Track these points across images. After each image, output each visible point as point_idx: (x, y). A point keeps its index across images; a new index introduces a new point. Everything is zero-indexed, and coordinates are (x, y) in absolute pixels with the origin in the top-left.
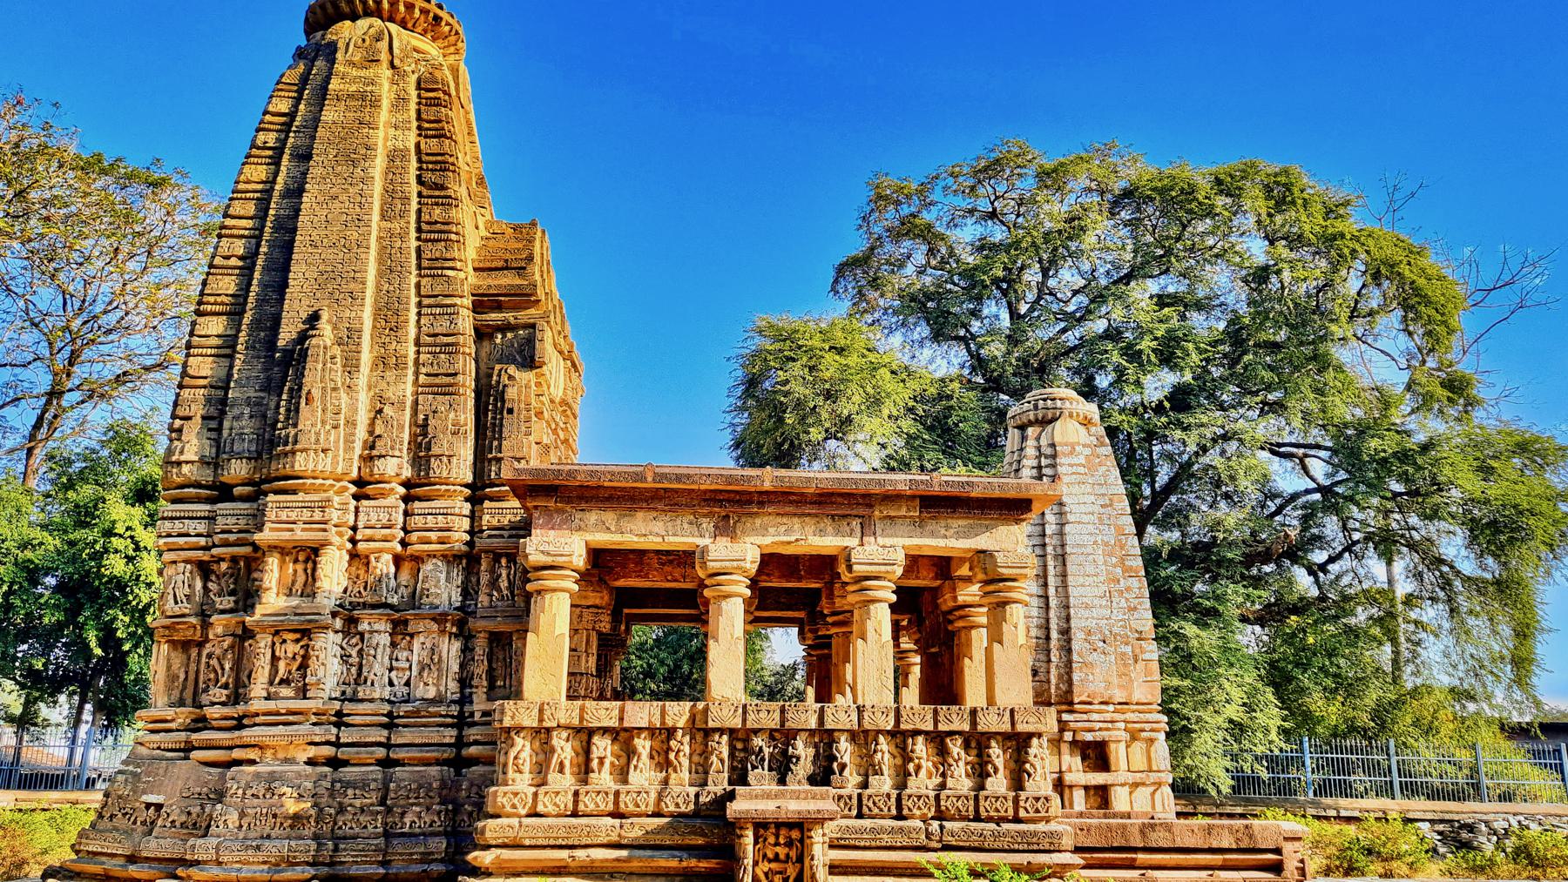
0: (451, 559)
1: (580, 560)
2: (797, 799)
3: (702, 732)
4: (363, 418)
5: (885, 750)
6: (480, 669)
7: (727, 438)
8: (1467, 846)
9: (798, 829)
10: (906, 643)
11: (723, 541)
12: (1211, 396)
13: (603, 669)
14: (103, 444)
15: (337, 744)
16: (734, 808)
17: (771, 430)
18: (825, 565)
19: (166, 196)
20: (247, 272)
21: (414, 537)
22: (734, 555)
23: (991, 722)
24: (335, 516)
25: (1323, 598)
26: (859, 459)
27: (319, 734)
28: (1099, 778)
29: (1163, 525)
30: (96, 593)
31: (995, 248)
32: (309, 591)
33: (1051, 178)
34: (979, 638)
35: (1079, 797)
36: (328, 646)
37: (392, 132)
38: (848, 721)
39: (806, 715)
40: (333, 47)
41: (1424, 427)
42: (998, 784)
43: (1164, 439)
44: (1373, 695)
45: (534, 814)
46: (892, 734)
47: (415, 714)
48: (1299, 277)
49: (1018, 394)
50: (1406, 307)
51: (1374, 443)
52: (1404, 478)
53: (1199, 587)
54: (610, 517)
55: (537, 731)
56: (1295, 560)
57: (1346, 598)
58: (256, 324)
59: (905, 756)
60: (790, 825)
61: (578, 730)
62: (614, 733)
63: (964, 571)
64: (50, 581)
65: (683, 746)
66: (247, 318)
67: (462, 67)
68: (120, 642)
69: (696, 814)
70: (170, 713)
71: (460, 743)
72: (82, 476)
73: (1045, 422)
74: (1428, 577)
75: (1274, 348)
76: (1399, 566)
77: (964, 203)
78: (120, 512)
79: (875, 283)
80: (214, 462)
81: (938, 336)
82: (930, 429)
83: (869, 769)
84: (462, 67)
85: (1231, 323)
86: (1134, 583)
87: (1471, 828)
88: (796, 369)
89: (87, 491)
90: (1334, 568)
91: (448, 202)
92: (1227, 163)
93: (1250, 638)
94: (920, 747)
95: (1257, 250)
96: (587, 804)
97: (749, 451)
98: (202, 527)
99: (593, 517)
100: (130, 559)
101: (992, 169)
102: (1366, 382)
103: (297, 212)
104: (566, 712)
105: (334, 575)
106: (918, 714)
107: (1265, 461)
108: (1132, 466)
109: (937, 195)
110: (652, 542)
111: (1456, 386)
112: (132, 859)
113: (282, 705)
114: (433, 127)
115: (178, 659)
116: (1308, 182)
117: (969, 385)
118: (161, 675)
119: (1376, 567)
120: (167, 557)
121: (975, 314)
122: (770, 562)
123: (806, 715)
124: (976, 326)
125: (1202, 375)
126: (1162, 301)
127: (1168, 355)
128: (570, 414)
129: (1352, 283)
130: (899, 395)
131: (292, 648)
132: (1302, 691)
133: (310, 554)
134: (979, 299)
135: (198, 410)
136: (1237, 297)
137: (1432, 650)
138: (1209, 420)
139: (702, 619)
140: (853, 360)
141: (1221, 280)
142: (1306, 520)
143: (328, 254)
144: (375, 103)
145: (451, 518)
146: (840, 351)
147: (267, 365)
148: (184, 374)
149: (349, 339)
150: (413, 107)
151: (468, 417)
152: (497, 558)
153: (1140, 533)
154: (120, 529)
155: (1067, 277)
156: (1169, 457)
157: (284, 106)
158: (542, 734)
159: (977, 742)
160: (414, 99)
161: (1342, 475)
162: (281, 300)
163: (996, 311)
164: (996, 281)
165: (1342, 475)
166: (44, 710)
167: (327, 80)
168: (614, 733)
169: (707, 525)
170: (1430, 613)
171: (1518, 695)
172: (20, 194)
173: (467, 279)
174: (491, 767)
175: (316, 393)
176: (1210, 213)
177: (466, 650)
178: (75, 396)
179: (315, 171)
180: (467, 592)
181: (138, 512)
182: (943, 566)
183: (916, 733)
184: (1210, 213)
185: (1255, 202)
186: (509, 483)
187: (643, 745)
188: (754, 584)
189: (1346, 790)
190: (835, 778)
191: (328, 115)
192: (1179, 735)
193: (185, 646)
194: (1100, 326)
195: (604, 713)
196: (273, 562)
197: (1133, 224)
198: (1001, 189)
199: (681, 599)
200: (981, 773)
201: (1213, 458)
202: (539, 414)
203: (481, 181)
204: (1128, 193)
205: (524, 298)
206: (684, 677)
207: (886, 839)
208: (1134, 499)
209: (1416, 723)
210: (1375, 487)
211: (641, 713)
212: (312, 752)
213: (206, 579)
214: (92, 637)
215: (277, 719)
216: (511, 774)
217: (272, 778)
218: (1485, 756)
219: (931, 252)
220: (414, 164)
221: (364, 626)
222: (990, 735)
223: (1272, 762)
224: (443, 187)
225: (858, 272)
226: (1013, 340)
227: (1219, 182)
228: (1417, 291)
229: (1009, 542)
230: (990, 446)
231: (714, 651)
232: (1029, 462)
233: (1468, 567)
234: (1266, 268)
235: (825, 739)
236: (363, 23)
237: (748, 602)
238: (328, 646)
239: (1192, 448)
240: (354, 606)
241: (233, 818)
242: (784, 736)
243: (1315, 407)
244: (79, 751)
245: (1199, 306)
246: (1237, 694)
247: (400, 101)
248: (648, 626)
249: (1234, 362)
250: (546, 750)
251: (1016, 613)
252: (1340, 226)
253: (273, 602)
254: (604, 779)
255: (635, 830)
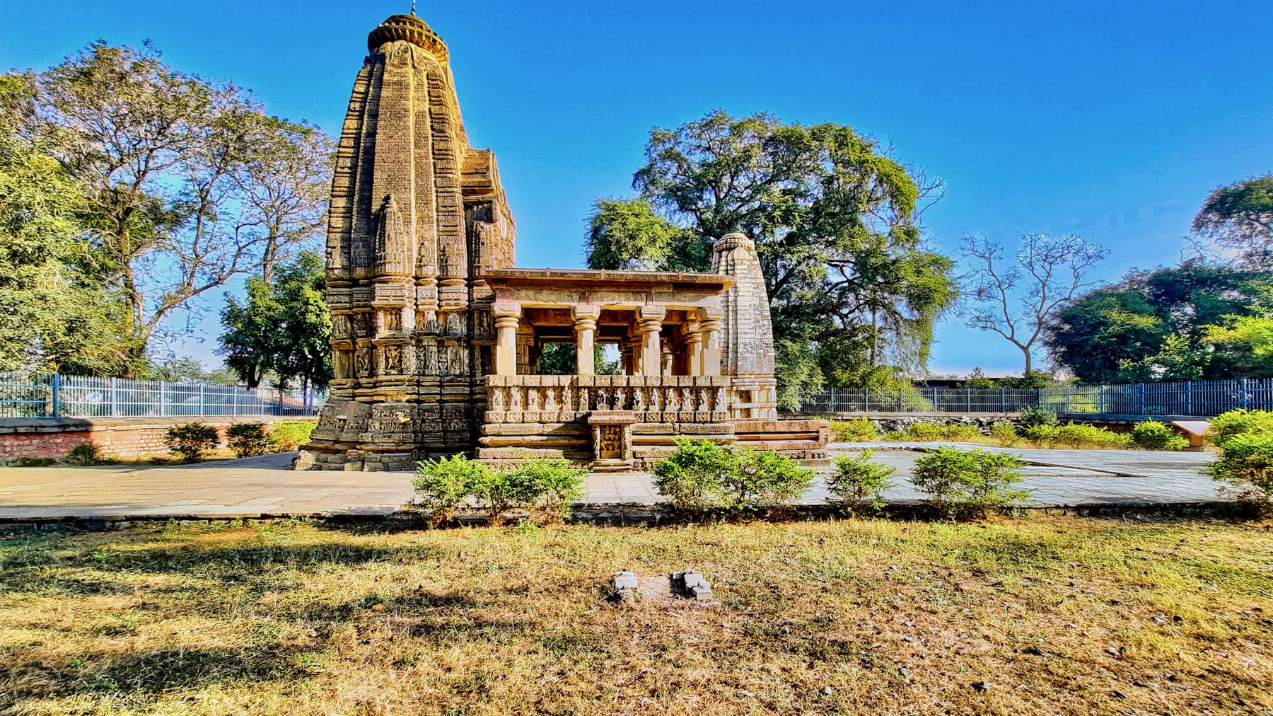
0: (461, 313)
1: (518, 313)
2: (618, 415)
3: (575, 388)
4: (415, 247)
5: (656, 396)
6: (478, 362)
7: (584, 258)
8: (893, 429)
9: (618, 428)
10: (666, 350)
11: (583, 304)
12: (804, 239)
13: (532, 362)
14: (298, 263)
15: (418, 394)
16: (591, 419)
17: (605, 251)
18: (630, 315)
19: (312, 139)
20: (353, 175)
21: (443, 303)
22: (588, 311)
23: (702, 382)
24: (407, 294)
25: (845, 329)
26: (648, 265)
27: (410, 390)
28: (747, 405)
29: (780, 298)
30: (304, 331)
31: (709, 165)
32: (399, 327)
33: (737, 130)
34: (698, 347)
35: (738, 412)
36: (410, 352)
37: (417, 103)
38: (641, 383)
39: (621, 380)
40: (383, 56)
41: (894, 253)
42: (704, 408)
43: (783, 259)
44: (862, 370)
45: (505, 422)
46: (659, 388)
47: (452, 381)
48: (846, 183)
49: (718, 237)
50: (892, 196)
51: (873, 260)
52: (884, 276)
53: (793, 325)
54: (531, 293)
55: (505, 388)
56: (835, 313)
57: (854, 329)
58: (360, 201)
59: (665, 397)
60: (616, 426)
61: (522, 388)
62: (538, 389)
63: (692, 317)
64: (284, 325)
65: (568, 394)
66: (356, 198)
67: (449, 68)
68: (319, 352)
69: (575, 422)
70: (344, 381)
71: (472, 393)
72: (290, 278)
73: (730, 249)
74: (890, 320)
75: (834, 216)
76: (878, 315)
77: (694, 142)
78: (310, 293)
79: (653, 182)
80: (348, 268)
81: (682, 208)
82: (678, 254)
83: (649, 402)
84: (449, 68)
85: (815, 203)
86: (766, 322)
87: (894, 422)
88: (616, 224)
89: (294, 284)
90: (851, 316)
91: (446, 139)
92: (818, 123)
93: (813, 346)
94: (671, 393)
95: (829, 167)
96: (528, 418)
97: (594, 262)
98: (347, 299)
99: (523, 293)
100: (318, 316)
101: (708, 125)
102: (872, 232)
103: (374, 144)
104: (516, 380)
105: (409, 321)
106: (670, 379)
107: (827, 268)
108: (768, 272)
109: (683, 138)
110: (550, 305)
111: (910, 234)
112: (336, 442)
113: (393, 378)
114: (436, 100)
115: (344, 358)
116: (856, 135)
117: (697, 232)
118: (338, 366)
119: (868, 315)
120: (334, 312)
121: (700, 198)
122: (605, 314)
123: (621, 380)
124: (700, 204)
125: (801, 228)
126: (785, 192)
127: (786, 220)
128: (514, 244)
129: (870, 184)
130: (664, 237)
131: (394, 353)
132: (833, 369)
133: (397, 311)
134: (702, 190)
135: (338, 244)
136: (819, 192)
137: (887, 351)
138: (804, 250)
139: (574, 340)
140: (643, 220)
141: (813, 184)
142: (841, 295)
143: (391, 166)
144: (407, 87)
145: (459, 295)
146: (637, 216)
147: (367, 225)
148: (330, 226)
149: (405, 209)
150: (426, 89)
151: (463, 247)
152: (481, 313)
153: (770, 301)
154: (311, 301)
155: (742, 180)
156: (784, 267)
157: (362, 89)
158: (506, 389)
159: (696, 391)
160: (426, 85)
161: (858, 275)
162: (371, 190)
163: (709, 197)
164: (710, 182)
165: (858, 275)
166: (290, 383)
167: (382, 75)
168: (538, 389)
169: (576, 296)
170: (888, 335)
171: (920, 368)
172: (240, 138)
173: (458, 179)
174: (485, 404)
175: (392, 235)
176: (809, 149)
177: (471, 354)
178: (282, 240)
179: (381, 123)
180: (470, 327)
181: (318, 294)
182: (683, 315)
183: (670, 387)
184: (809, 149)
185: (830, 144)
186: (485, 277)
187: (551, 394)
188: (597, 324)
189: (847, 409)
190: (635, 407)
191: (384, 93)
192: (781, 387)
193: (347, 352)
194: (756, 205)
195: (533, 380)
196: (381, 315)
197: (774, 154)
198: (713, 135)
199: (568, 335)
200: (697, 403)
201: (803, 267)
202: (496, 245)
203: (462, 129)
204: (771, 139)
205: (486, 188)
206: (567, 364)
207: (656, 431)
208: (768, 285)
209: (878, 381)
210: (872, 280)
211: (549, 380)
212: (408, 397)
213: (352, 323)
214: (306, 351)
215: (390, 383)
216: (494, 406)
217: (392, 408)
218: (903, 394)
219: (680, 167)
220: (428, 119)
221: (425, 343)
222: (702, 388)
223: (819, 398)
224: (443, 132)
225: (645, 176)
226: (717, 211)
227: (814, 134)
228: (898, 188)
229: (712, 304)
230: (704, 263)
231: (580, 354)
232: (722, 268)
233: (906, 315)
234: (832, 177)
235: (629, 391)
236: (398, 43)
237: (595, 332)
238: (410, 352)
239: (794, 262)
240: (420, 334)
241: (377, 425)
242: (612, 390)
243: (849, 243)
244: (308, 399)
245: (801, 195)
246: (806, 371)
247: (419, 87)
248: (549, 343)
249: (815, 223)
250: (509, 396)
251: (714, 335)
252: (867, 156)
253: (383, 332)
254: (534, 407)
255: (549, 429)
